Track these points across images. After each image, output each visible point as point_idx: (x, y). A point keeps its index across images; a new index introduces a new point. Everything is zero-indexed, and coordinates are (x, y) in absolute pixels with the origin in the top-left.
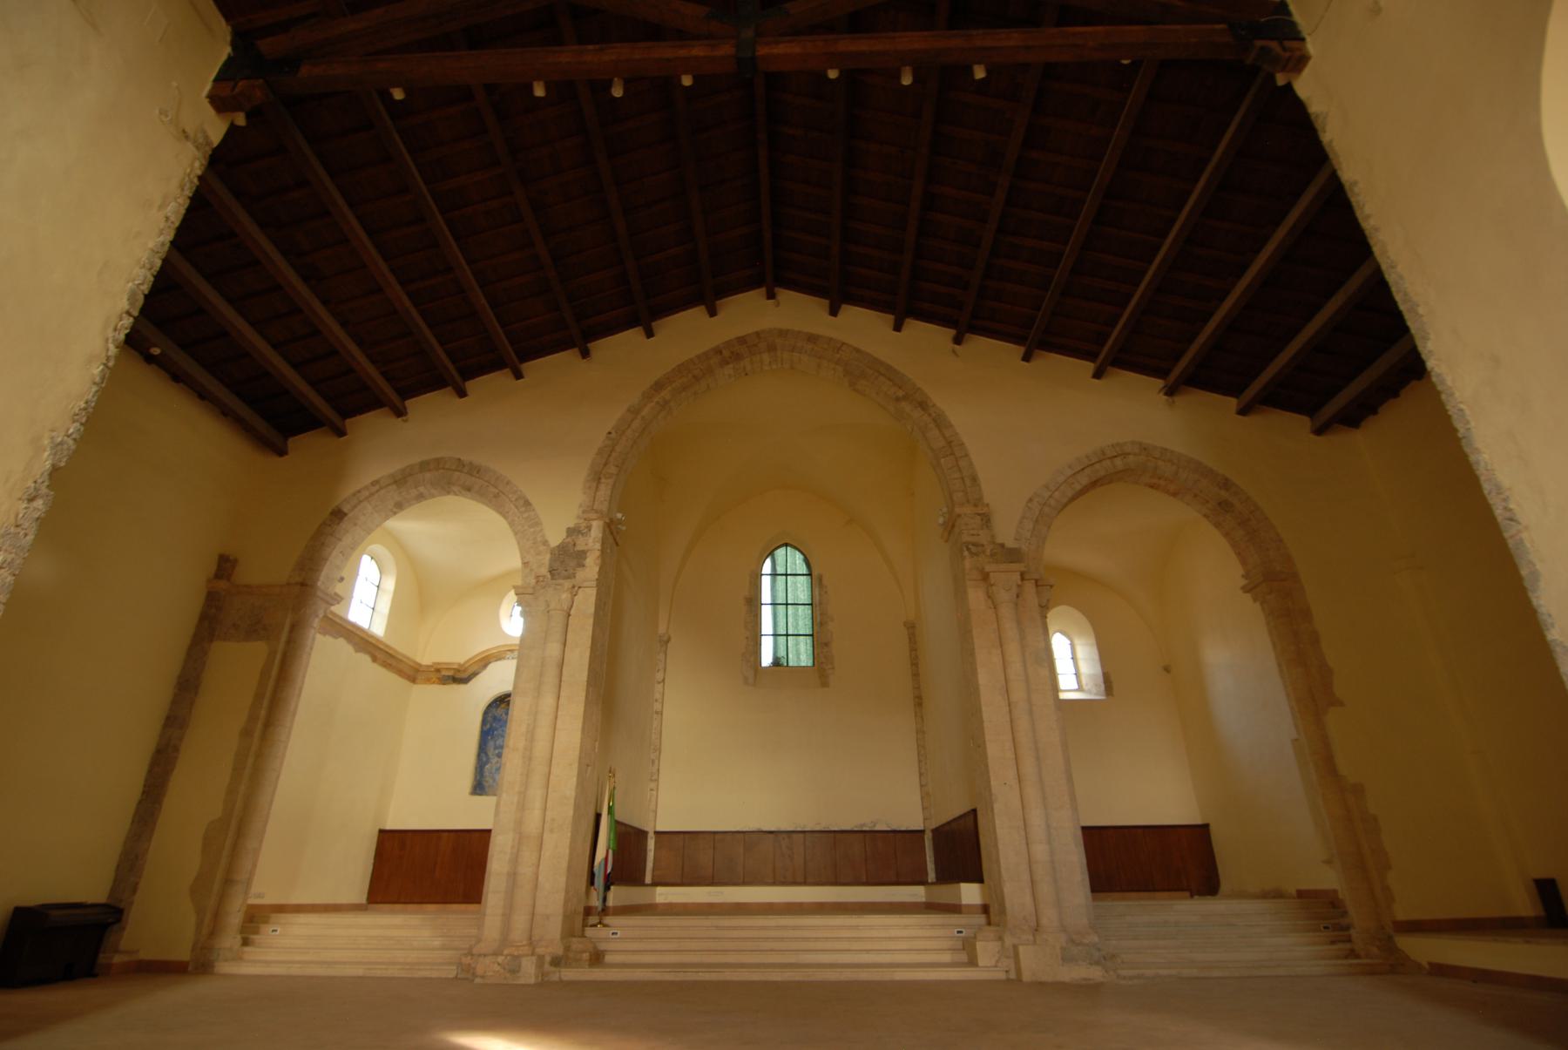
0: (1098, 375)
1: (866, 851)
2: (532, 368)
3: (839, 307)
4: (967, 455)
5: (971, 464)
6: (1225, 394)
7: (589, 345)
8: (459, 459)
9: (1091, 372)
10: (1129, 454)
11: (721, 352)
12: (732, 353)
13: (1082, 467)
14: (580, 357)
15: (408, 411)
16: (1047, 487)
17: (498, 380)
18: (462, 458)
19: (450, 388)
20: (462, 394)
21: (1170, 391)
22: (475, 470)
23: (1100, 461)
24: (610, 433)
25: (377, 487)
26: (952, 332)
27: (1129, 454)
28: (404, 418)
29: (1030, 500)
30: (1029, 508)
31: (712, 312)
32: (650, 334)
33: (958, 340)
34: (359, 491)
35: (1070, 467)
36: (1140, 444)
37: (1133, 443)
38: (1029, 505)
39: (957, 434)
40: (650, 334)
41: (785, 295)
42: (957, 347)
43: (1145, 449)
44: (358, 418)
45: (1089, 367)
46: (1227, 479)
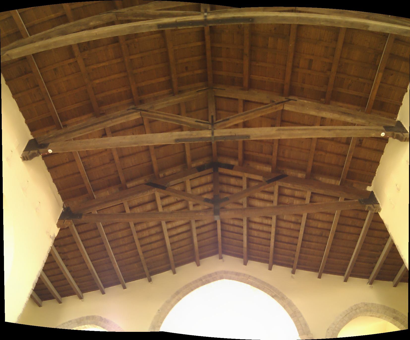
0: (346, 280)
1: (253, 243)
2: (129, 285)
3: (247, 262)
4: (302, 316)
5: (304, 319)
6: (383, 280)
7: (151, 277)
8: (101, 317)
9: (343, 280)
10: (361, 307)
11: (202, 280)
12: (206, 280)
13: (345, 315)
14: (148, 281)
15: (84, 297)
16: (333, 324)
17: (117, 288)
18: (102, 317)
19: (99, 290)
20: (103, 293)
21: (371, 283)
22: (223, 208)
23: (351, 312)
24: (159, 310)
25: (71, 323)
26: (291, 269)
27: (361, 307)
28: (82, 300)
29: (328, 329)
30: (328, 332)
31: (198, 265)
32: (174, 273)
33: (293, 272)
34: (64, 323)
35: (341, 315)
36: (364, 303)
37: (362, 303)
38: (328, 331)
39: (297, 308)
40: (174, 273)
41: (227, 258)
42: (293, 275)
43: (366, 305)
44: (66, 298)
45: (342, 278)
46: (394, 310)
